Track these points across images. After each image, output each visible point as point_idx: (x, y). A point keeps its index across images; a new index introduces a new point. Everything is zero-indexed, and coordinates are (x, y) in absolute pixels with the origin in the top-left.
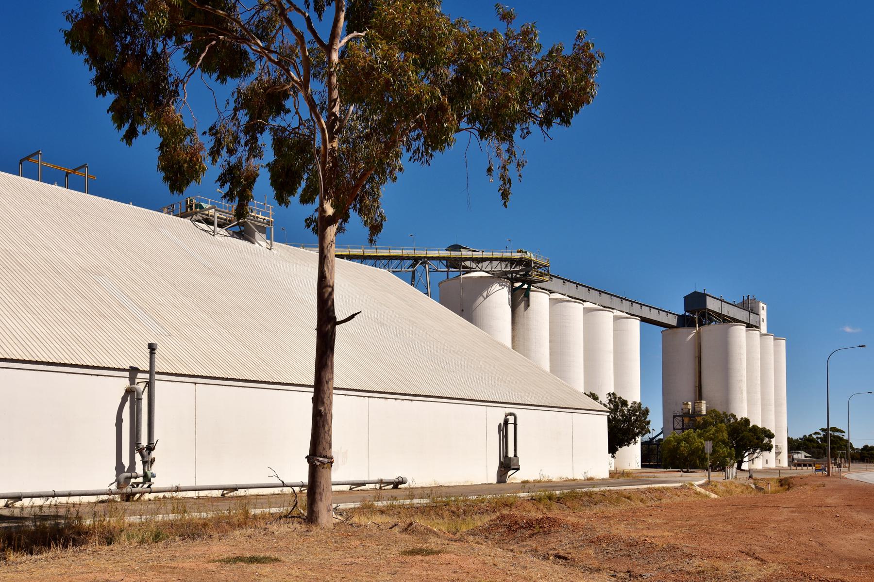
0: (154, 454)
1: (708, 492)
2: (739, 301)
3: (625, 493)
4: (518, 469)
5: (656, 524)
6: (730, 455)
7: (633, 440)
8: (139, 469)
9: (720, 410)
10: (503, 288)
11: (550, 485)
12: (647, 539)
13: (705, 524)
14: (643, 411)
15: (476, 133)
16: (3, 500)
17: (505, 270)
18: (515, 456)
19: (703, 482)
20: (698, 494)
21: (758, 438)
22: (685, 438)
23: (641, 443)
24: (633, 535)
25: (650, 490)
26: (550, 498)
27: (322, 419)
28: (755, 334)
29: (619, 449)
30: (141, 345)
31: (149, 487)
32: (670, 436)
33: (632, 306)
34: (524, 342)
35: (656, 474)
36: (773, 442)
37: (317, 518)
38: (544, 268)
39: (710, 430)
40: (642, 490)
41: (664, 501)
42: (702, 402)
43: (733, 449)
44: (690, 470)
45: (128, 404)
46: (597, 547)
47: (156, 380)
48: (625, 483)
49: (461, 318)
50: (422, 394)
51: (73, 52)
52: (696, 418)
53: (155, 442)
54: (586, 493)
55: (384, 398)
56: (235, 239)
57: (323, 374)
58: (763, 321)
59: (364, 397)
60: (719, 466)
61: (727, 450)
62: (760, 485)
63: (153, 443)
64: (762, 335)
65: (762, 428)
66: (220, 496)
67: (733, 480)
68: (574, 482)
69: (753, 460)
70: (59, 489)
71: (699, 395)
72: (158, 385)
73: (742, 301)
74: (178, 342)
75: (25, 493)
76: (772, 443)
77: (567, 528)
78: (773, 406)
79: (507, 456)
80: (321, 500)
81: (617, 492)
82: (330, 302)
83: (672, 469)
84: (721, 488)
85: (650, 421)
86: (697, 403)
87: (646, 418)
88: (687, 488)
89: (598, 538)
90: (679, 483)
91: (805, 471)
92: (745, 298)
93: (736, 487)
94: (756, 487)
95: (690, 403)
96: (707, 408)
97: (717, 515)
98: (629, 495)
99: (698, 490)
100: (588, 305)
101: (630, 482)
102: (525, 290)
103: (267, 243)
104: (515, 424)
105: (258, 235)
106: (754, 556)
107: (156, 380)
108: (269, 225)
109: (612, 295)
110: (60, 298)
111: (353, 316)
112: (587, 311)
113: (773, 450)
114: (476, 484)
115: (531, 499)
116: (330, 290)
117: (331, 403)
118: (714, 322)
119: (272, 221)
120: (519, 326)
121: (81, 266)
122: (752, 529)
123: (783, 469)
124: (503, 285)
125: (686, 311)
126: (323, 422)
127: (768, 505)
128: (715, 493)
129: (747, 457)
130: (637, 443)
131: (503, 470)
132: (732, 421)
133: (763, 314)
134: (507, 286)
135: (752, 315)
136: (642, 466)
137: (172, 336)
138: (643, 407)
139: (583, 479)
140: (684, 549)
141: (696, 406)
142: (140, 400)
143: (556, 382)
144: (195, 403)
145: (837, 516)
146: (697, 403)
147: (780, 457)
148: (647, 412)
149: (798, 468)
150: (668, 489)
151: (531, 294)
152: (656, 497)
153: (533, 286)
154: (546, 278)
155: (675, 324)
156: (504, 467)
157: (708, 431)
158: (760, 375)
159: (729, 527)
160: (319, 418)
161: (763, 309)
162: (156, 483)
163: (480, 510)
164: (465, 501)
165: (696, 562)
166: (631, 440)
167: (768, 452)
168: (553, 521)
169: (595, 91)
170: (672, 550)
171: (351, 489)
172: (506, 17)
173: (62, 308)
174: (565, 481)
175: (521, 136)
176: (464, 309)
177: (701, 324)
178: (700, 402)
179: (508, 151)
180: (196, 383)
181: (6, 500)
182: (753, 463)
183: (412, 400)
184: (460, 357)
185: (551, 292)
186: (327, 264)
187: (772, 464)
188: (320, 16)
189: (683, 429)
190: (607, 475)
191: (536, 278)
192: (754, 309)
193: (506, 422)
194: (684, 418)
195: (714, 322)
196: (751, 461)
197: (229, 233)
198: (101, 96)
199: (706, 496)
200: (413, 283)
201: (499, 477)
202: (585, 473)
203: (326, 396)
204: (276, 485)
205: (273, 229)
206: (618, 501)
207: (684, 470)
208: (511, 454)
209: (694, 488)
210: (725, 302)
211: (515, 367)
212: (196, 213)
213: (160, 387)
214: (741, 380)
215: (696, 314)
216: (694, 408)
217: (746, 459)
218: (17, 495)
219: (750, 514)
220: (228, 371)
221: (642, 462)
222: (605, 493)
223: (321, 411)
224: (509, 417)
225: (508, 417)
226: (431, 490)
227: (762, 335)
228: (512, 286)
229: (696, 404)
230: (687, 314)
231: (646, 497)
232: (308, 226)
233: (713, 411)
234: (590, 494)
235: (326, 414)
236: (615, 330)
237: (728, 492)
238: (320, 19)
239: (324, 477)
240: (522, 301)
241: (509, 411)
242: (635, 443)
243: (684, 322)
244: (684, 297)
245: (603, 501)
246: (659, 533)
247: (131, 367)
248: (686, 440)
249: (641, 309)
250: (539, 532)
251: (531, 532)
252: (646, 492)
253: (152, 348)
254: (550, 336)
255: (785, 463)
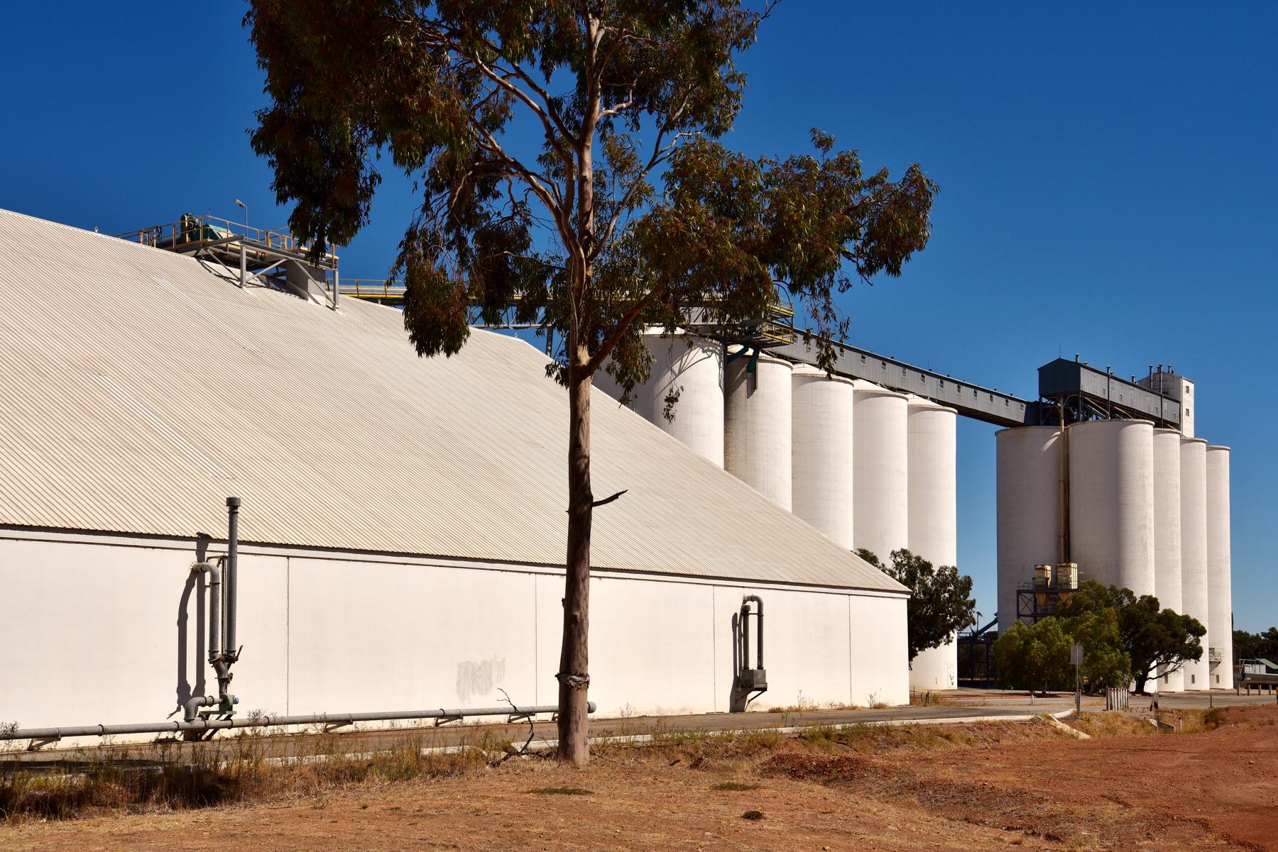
0: (234, 668)
1: (1075, 730)
2: (1142, 374)
3: (941, 730)
4: (764, 690)
5: (995, 769)
6: (1121, 665)
7: (945, 637)
8: (212, 689)
9: (1104, 580)
10: (709, 357)
11: (814, 715)
12: (986, 783)
13: (1063, 769)
14: (961, 582)
15: (786, 286)
16: (26, 740)
17: (712, 323)
18: (760, 667)
19: (1067, 713)
20: (1058, 733)
21: (1174, 635)
22: (1040, 633)
23: (958, 639)
24: (968, 780)
25: (980, 726)
26: (827, 736)
27: (578, 627)
28: (1173, 438)
29: (919, 653)
30: (198, 495)
31: (228, 718)
32: (1012, 630)
33: (942, 386)
34: (746, 455)
35: (988, 700)
36: (1205, 642)
37: (573, 752)
38: (783, 320)
39: (1087, 619)
40: (967, 725)
41: (1004, 742)
42: (1070, 566)
43: (1127, 653)
44: (1047, 692)
45: (194, 591)
46: (921, 794)
47: (239, 553)
48: (939, 713)
49: (634, 413)
50: (616, 567)
51: (257, 155)
52: (1060, 594)
53: (237, 649)
54: (881, 729)
55: (559, 574)
56: (274, 291)
57: (578, 569)
58: (1188, 414)
59: (530, 573)
60: (1099, 685)
61: (1116, 656)
62: (1167, 720)
63: (235, 651)
64: (1184, 441)
65: (1183, 617)
66: (550, 720)
67: (1120, 711)
68: (853, 712)
69: (1166, 675)
70: (108, 723)
71: (1066, 553)
72: (241, 560)
73: (1148, 375)
74: (249, 489)
75: (64, 728)
76: (1201, 644)
77: (876, 772)
78: (1206, 575)
79: (746, 667)
80: (577, 731)
81: (928, 728)
82: (586, 477)
83: (1014, 689)
84: (1097, 724)
85: (974, 601)
86: (1062, 566)
87: (967, 595)
88: (1041, 722)
89: (921, 783)
90: (1028, 714)
91: (1265, 697)
92: (1154, 370)
93: (1124, 723)
94: (1160, 724)
95: (1049, 568)
96: (1080, 577)
97: (1082, 760)
98: (948, 733)
99: (1059, 727)
100: (861, 385)
101: (946, 713)
102: (748, 360)
103: (327, 297)
104: (760, 615)
105: (312, 284)
106: (1117, 801)
107: (239, 553)
108: (331, 267)
109: (905, 367)
110: (62, 419)
111: (616, 497)
112: (860, 396)
113: (1205, 657)
114: (698, 713)
115: (799, 737)
116: (586, 460)
117: (587, 607)
118: (1094, 417)
119: (336, 260)
120: (737, 425)
121: (68, 358)
122: (1125, 776)
123: (1222, 692)
124: (709, 350)
125: (1042, 395)
126: (579, 631)
127: (1161, 749)
128: (1087, 732)
129: (1155, 670)
130: (951, 641)
131: (740, 690)
132: (1126, 602)
133: (1188, 400)
134: (716, 353)
135: (1166, 403)
136: (960, 684)
137: (237, 479)
138: (961, 575)
139: (868, 706)
140: (1034, 794)
141: (1059, 574)
142: (217, 586)
143: (821, 540)
144: (287, 587)
145: (1250, 763)
146: (1062, 566)
147: (1218, 670)
148: (967, 585)
149: (1252, 691)
150: (1009, 723)
151: (760, 366)
152: (991, 736)
153: (763, 352)
154: (787, 338)
155: (1021, 420)
156: (742, 686)
157: (1082, 622)
158: (1179, 517)
159: (1096, 773)
160: (573, 626)
161: (1188, 391)
162: (241, 713)
163: (727, 752)
164: (703, 738)
165: (1047, 807)
166: (942, 637)
167: (1193, 661)
168: (856, 764)
169: (928, 232)
170: (1018, 795)
171: (510, 721)
172: (824, 143)
173: (71, 437)
174: (838, 709)
175: (839, 290)
176: (638, 395)
177: (1070, 420)
178: (1067, 566)
179: (825, 307)
180: (288, 557)
181: (30, 740)
182: (1167, 681)
183: (600, 577)
184: (663, 500)
185: (795, 361)
186: (582, 428)
187: (1204, 684)
188: (547, 78)
189: (1035, 617)
190: (905, 700)
191: (768, 337)
192: (1171, 391)
193: (745, 611)
194: (1036, 596)
195: (1094, 417)
196: (1163, 678)
197: (261, 281)
198: (281, 204)
199: (1072, 736)
200: (549, 348)
201: (734, 702)
202: (871, 697)
203: (582, 597)
204: (405, 715)
205: (337, 273)
206: (931, 741)
207: (1036, 692)
208: (753, 665)
209: (1053, 723)
210: (1115, 378)
211: (752, 515)
212: (205, 246)
213: (245, 564)
214: (1145, 526)
215: (1062, 400)
216: (1055, 576)
217: (1153, 674)
218: (52, 732)
219: (1130, 758)
220: (333, 536)
221: (959, 676)
222: (910, 729)
223: (576, 616)
224: (749, 603)
225: (749, 603)
226: (658, 722)
227: (1184, 441)
228: (726, 350)
229: (1060, 569)
230: (1044, 400)
231: (975, 736)
232: (549, 374)
233: (1092, 584)
234: (887, 731)
235: (582, 621)
236: (911, 431)
237: (1108, 730)
238: (548, 81)
239: (581, 700)
240: (742, 379)
241: (749, 593)
242: (949, 642)
243: (1039, 415)
244: (1038, 369)
245: (908, 742)
246: (1001, 777)
247: (198, 533)
248: (1041, 636)
249: (959, 391)
250: (837, 778)
251: (826, 778)
252: (975, 729)
253: (233, 504)
254: (793, 443)
255: (1228, 683)
